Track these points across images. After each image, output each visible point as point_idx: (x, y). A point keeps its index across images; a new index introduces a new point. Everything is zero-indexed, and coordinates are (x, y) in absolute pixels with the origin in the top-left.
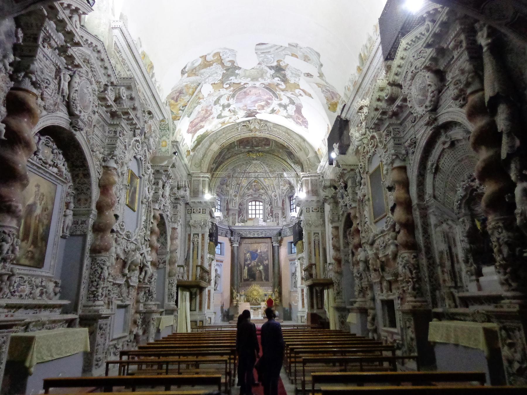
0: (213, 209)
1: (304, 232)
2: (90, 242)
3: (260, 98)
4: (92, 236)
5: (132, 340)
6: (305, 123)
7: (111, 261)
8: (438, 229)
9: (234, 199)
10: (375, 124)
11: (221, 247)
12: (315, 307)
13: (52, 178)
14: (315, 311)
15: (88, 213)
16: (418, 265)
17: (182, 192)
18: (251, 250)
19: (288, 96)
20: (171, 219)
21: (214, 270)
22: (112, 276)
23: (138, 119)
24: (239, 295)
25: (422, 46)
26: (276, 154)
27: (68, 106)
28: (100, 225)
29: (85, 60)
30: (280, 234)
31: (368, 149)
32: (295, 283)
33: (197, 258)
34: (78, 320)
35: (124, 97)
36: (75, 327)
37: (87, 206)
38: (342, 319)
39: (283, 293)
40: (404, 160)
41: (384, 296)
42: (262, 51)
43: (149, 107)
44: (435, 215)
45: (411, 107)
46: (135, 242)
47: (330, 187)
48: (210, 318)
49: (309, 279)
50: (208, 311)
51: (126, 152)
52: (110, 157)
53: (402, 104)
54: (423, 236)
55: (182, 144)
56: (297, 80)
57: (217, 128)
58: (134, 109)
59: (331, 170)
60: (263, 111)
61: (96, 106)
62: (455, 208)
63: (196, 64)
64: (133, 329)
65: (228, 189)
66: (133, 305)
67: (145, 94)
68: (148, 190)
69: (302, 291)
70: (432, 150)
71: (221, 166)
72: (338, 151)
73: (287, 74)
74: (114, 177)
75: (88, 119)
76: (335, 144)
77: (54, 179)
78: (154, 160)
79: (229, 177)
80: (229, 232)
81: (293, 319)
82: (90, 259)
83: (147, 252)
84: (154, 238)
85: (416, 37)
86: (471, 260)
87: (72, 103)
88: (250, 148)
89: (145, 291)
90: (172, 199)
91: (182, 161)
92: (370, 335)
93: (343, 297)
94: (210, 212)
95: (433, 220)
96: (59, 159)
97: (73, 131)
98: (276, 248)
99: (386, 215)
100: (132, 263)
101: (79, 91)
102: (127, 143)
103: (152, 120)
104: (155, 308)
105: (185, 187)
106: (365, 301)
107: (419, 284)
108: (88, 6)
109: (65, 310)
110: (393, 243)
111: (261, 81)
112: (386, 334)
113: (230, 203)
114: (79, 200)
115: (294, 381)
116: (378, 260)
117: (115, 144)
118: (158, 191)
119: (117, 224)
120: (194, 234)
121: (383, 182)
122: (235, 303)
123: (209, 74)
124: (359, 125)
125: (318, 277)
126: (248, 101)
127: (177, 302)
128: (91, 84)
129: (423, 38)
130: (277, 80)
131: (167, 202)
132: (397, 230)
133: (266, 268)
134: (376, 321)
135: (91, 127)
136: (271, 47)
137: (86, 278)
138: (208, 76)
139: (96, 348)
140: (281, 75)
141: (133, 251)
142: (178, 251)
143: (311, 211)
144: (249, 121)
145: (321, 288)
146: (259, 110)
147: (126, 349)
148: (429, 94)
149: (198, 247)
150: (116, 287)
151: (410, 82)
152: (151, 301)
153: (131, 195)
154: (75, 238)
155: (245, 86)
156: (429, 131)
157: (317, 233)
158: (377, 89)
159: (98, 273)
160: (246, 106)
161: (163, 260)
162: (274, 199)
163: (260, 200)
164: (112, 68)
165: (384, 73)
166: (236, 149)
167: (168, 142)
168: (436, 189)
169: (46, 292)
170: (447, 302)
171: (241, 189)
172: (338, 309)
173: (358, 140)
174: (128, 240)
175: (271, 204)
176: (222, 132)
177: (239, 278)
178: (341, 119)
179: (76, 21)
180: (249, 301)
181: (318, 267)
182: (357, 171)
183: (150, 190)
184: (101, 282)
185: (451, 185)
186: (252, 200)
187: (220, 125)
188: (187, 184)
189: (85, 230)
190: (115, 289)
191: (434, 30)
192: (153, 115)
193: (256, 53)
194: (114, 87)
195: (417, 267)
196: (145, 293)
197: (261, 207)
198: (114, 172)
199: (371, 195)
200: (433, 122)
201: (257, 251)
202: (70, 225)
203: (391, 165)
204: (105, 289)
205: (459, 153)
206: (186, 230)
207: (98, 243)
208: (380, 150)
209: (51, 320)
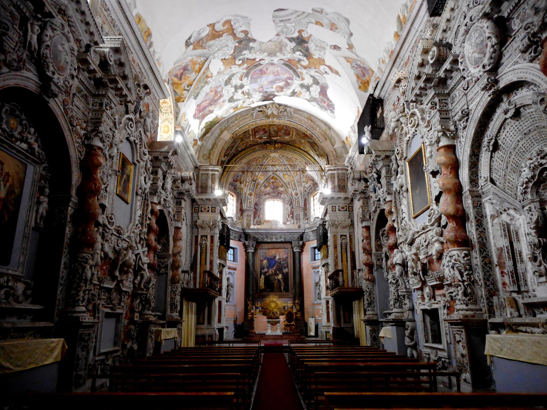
1: (329, 235)
3: (278, 77)
6: (330, 107)
7: (95, 259)
8: (496, 221)
9: (249, 198)
13: (20, 155)
16: (471, 266)
18: (268, 257)
20: (174, 217)
21: (226, 279)
23: (129, 89)
26: (298, 146)
30: (301, 237)
31: (407, 129)
33: (206, 264)
35: (111, 61)
43: (144, 80)
45: (464, 69)
52: (94, 134)
54: (477, 229)
56: (322, 54)
57: (228, 114)
58: (125, 77)
59: (361, 161)
60: (282, 93)
61: (75, 69)
62: (519, 194)
63: (203, 35)
65: (242, 186)
66: (126, 314)
68: (145, 180)
69: (327, 302)
71: (234, 159)
73: (310, 48)
74: (99, 158)
75: (64, 83)
79: (243, 172)
80: (243, 236)
83: (144, 252)
84: (153, 237)
86: (540, 258)
90: (175, 193)
91: (188, 151)
92: (409, 351)
93: (375, 309)
94: (220, 211)
95: (488, 210)
96: (29, 133)
98: (297, 255)
104: (152, 319)
109: (36, 316)
111: (280, 56)
112: (428, 351)
116: (419, 262)
117: (99, 119)
120: (202, 236)
123: (219, 47)
125: (346, 286)
126: (264, 81)
128: (69, 41)
130: (298, 55)
131: (167, 195)
132: (443, 223)
133: (286, 277)
138: (217, 49)
142: (183, 253)
144: (266, 106)
146: (278, 92)
150: (104, 292)
152: (149, 310)
155: (261, 62)
156: (486, 98)
160: (262, 87)
166: (251, 139)
168: (494, 172)
169: (14, 294)
170: (509, 310)
171: (257, 186)
176: (234, 119)
178: (374, 98)
181: (345, 275)
182: (393, 158)
183: (147, 180)
185: (514, 165)
187: (232, 111)
193: (274, 21)
195: (470, 268)
201: (275, 257)
202: (45, 214)
203: (436, 145)
204: (87, 292)
205: (526, 124)
208: (422, 129)
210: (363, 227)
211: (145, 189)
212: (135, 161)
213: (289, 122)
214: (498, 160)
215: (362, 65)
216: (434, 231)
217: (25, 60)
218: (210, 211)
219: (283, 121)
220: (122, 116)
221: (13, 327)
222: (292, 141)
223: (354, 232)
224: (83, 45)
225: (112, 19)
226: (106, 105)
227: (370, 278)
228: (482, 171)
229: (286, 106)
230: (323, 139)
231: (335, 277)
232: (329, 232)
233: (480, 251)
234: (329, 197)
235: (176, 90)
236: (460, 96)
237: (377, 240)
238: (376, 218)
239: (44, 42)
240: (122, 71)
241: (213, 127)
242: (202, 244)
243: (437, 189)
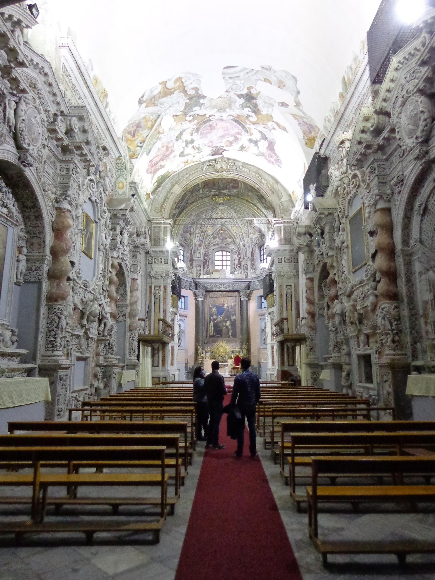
0: (176, 259)
1: (275, 285)
2: (45, 290)
4: (48, 283)
5: (94, 393)
6: (278, 161)
7: (68, 311)
8: (423, 277)
9: (199, 248)
10: (357, 160)
11: (184, 301)
12: (286, 364)
14: (286, 369)
15: (42, 259)
17: (141, 240)
18: (217, 305)
20: (131, 269)
21: (178, 326)
22: (70, 327)
24: (204, 352)
25: (416, 63)
26: (246, 198)
27: (15, 138)
28: (56, 271)
29: (31, 85)
30: (248, 287)
31: (349, 190)
33: (159, 312)
34: (37, 370)
35: (76, 129)
36: (35, 377)
37: (40, 251)
40: (389, 201)
41: (362, 351)
42: (231, 76)
44: (420, 262)
45: (400, 139)
46: (92, 292)
47: (305, 234)
48: (174, 375)
49: (280, 334)
50: (172, 367)
51: (80, 193)
52: (63, 197)
53: (389, 136)
54: (406, 285)
55: (141, 187)
56: (270, 110)
57: (179, 169)
58: (88, 143)
61: (46, 139)
63: (156, 92)
64: (94, 383)
65: (192, 237)
66: (93, 358)
67: (98, 126)
68: (105, 236)
69: (273, 347)
70: (421, 189)
71: (184, 211)
72: (315, 193)
73: (258, 104)
74: (68, 220)
75: (37, 153)
76: (311, 185)
77: (5, 221)
78: (110, 203)
79: (193, 224)
80: (193, 285)
82: (46, 308)
83: (106, 302)
84: (113, 289)
85: (410, 54)
87: (19, 134)
88: (216, 191)
89: (105, 344)
90: (131, 247)
91: (142, 205)
93: (317, 353)
94: (172, 262)
95: (417, 267)
96: (8, 199)
97: (22, 166)
98: (245, 303)
99: (366, 264)
100: (90, 313)
101: (26, 121)
102: (81, 183)
103: (107, 157)
104: (115, 362)
105: (145, 233)
106: (340, 357)
107: (399, 337)
108: (32, 17)
109: (24, 359)
110: (372, 294)
111: (229, 112)
112: (362, 390)
114: (32, 244)
115: (262, 434)
116: (355, 313)
117: (67, 183)
118: (116, 238)
119: (73, 271)
120: (155, 286)
121: (365, 226)
122: (200, 360)
124: (340, 163)
125: (290, 332)
127: (138, 356)
128: (39, 113)
129: (417, 55)
130: (247, 111)
131: (125, 249)
132: (377, 279)
133: (233, 324)
134: (351, 377)
135: (41, 163)
136: (241, 71)
137: (44, 327)
138: (168, 106)
139: (57, 398)
140: (251, 104)
141: (91, 301)
142: (139, 303)
143: (283, 261)
145: (293, 344)
146: (227, 146)
147: (87, 400)
148: (421, 122)
150: (75, 338)
151: (400, 109)
153: (86, 240)
154: (31, 285)
155: (211, 118)
156: (419, 167)
158: (361, 119)
159: (56, 322)
161: (123, 312)
162: (243, 249)
163: (227, 250)
164: (62, 95)
165: (370, 100)
167: (125, 184)
168: (423, 233)
171: (206, 237)
172: (311, 365)
174: (85, 290)
176: (185, 173)
179: (18, 36)
181: (289, 322)
182: (336, 215)
183: (107, 236)
184: (59, 332)
186: (217, 250)
187: (183, 165)
188: (147, 231)
189: (40, 277)
190: (74, 340)
191: (431, 43)
192: (108, 151)
193: (224, 78)
194: (64, 117)
195: (399, 319)
196: (105, 346)
197: (229, 258)
198: (68, 214)
199: (350, 241)
200: (424, 156)
201: (224, 305)
202: (24, 271)
203: (374, 207)
206: (146, 282)
207: (54, 291)
208: (363, 191)
209: (10, 369)
211: (106, 245)
212: (97, 219)
213: (237, 176)
214: (427, 223)
215: (308, 123)
216: (370, 285)
217: (5, 135)
218: (163, 263)
219: (232, 175)
220: (85, 178)
221: (7, 368)
222: (241, 194)
223: (298, 283)
224: (51, 115)
225: (73, 85)
226: (73, 170)
227: (312, 325)
228: (413, 233)
230: (271, 193)
231: (280, 325)
232: (275, 282)
233: (408, 303)
235: (129, 146)
236: (396, 162)
237: (320, 290)
239: (20, 116)
240: (85, 137)
242: (156, 293)
243: (374, 247)
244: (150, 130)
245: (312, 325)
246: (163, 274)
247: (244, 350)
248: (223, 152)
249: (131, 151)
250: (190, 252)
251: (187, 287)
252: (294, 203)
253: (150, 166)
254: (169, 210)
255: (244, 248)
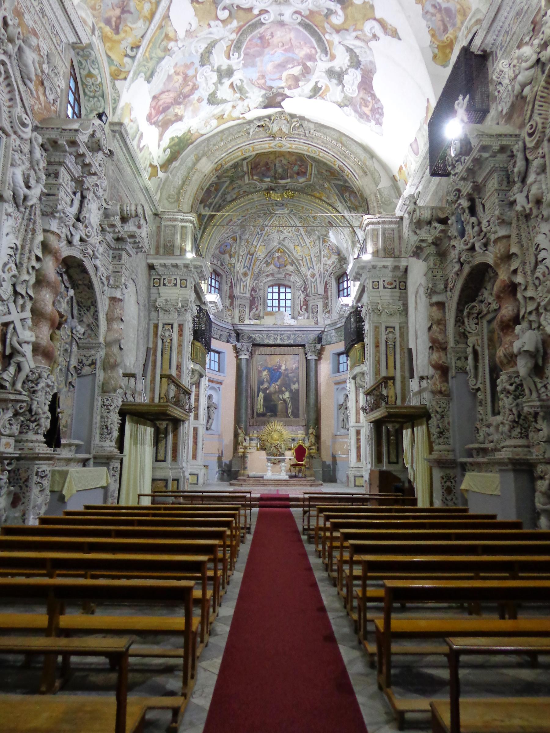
3: (290, 55)
9: (244, 280)
12: (385, 460)
14: (384, 468)
18: (270, 366)
19: (347, 43)
20: (108, 278)
24: (247, 438)
30: (319, 340)
32: (346, 419)
38: (448, 484)
39: (323, 438)
50: (194, 462)
57: (208, 129)
60: (296, 92)
65: (233, 261)
69: (358, 433)
80: (234, 335)
81: (338, 481)
88: (271, 182)
90: (109, 237)
93: (451, 441)
94: (195, 286)
98: (313, 364)
105: (137, 216)
113: (236, 285)
118: (56, 192)
133: (295, 396)
143: (381, 287)
144: (269, 117)
145: (397, 426)
146: (289, 88)
149: (171, 348)
155: (262, 17)
157: (391, 327)
161: (91, 358)
162: (311, 281)
166: (247, 181)
171: (255, 263)
173: (529, 64)
175: (305, 290)
176: (219, 139)
177: (249, 411)
180: (265, 449)
197: (289, 296)
201: (280, 367)
206: (149, 317)
210: (432, 305)
223: (407, 323)
227: (443, 389)
229: (302, 118)
230: (361, 173)
234: (370, 266)
235: (110, 54)
237: (459, 324)
238: (459, 286)
241: (183, 149)
242: (164, 336)
244: (147, 23)
245: (443, 389)
246: (177, 303)
247: (311, 436)
248: (283, 100)
249: (113, 64)
250: (229, 285)
251: (224, 338)
252: (402, 189)
253: (154, 108)
254: (191, 199)
255: (313, 280)
